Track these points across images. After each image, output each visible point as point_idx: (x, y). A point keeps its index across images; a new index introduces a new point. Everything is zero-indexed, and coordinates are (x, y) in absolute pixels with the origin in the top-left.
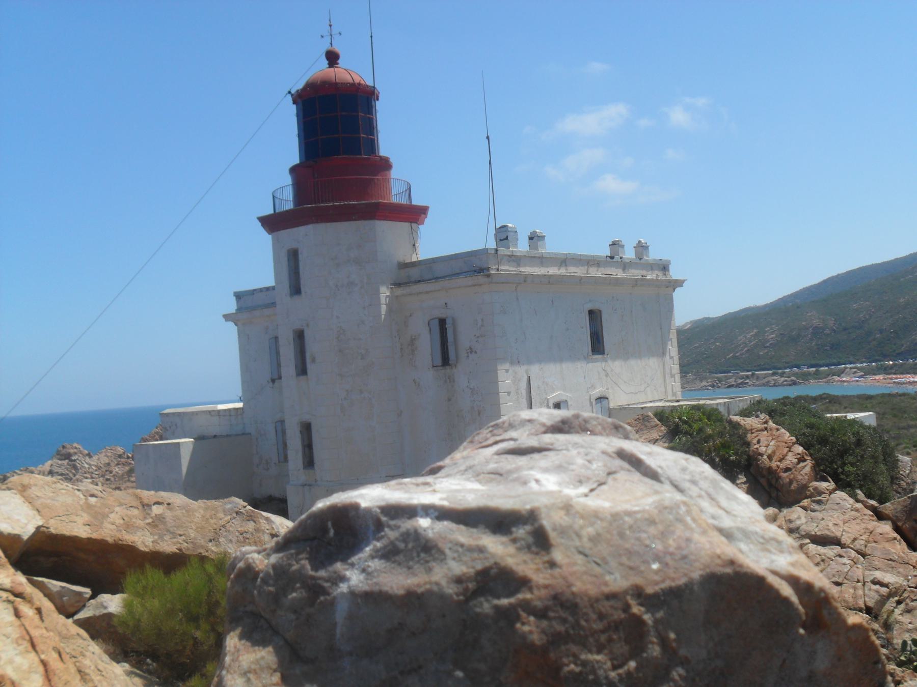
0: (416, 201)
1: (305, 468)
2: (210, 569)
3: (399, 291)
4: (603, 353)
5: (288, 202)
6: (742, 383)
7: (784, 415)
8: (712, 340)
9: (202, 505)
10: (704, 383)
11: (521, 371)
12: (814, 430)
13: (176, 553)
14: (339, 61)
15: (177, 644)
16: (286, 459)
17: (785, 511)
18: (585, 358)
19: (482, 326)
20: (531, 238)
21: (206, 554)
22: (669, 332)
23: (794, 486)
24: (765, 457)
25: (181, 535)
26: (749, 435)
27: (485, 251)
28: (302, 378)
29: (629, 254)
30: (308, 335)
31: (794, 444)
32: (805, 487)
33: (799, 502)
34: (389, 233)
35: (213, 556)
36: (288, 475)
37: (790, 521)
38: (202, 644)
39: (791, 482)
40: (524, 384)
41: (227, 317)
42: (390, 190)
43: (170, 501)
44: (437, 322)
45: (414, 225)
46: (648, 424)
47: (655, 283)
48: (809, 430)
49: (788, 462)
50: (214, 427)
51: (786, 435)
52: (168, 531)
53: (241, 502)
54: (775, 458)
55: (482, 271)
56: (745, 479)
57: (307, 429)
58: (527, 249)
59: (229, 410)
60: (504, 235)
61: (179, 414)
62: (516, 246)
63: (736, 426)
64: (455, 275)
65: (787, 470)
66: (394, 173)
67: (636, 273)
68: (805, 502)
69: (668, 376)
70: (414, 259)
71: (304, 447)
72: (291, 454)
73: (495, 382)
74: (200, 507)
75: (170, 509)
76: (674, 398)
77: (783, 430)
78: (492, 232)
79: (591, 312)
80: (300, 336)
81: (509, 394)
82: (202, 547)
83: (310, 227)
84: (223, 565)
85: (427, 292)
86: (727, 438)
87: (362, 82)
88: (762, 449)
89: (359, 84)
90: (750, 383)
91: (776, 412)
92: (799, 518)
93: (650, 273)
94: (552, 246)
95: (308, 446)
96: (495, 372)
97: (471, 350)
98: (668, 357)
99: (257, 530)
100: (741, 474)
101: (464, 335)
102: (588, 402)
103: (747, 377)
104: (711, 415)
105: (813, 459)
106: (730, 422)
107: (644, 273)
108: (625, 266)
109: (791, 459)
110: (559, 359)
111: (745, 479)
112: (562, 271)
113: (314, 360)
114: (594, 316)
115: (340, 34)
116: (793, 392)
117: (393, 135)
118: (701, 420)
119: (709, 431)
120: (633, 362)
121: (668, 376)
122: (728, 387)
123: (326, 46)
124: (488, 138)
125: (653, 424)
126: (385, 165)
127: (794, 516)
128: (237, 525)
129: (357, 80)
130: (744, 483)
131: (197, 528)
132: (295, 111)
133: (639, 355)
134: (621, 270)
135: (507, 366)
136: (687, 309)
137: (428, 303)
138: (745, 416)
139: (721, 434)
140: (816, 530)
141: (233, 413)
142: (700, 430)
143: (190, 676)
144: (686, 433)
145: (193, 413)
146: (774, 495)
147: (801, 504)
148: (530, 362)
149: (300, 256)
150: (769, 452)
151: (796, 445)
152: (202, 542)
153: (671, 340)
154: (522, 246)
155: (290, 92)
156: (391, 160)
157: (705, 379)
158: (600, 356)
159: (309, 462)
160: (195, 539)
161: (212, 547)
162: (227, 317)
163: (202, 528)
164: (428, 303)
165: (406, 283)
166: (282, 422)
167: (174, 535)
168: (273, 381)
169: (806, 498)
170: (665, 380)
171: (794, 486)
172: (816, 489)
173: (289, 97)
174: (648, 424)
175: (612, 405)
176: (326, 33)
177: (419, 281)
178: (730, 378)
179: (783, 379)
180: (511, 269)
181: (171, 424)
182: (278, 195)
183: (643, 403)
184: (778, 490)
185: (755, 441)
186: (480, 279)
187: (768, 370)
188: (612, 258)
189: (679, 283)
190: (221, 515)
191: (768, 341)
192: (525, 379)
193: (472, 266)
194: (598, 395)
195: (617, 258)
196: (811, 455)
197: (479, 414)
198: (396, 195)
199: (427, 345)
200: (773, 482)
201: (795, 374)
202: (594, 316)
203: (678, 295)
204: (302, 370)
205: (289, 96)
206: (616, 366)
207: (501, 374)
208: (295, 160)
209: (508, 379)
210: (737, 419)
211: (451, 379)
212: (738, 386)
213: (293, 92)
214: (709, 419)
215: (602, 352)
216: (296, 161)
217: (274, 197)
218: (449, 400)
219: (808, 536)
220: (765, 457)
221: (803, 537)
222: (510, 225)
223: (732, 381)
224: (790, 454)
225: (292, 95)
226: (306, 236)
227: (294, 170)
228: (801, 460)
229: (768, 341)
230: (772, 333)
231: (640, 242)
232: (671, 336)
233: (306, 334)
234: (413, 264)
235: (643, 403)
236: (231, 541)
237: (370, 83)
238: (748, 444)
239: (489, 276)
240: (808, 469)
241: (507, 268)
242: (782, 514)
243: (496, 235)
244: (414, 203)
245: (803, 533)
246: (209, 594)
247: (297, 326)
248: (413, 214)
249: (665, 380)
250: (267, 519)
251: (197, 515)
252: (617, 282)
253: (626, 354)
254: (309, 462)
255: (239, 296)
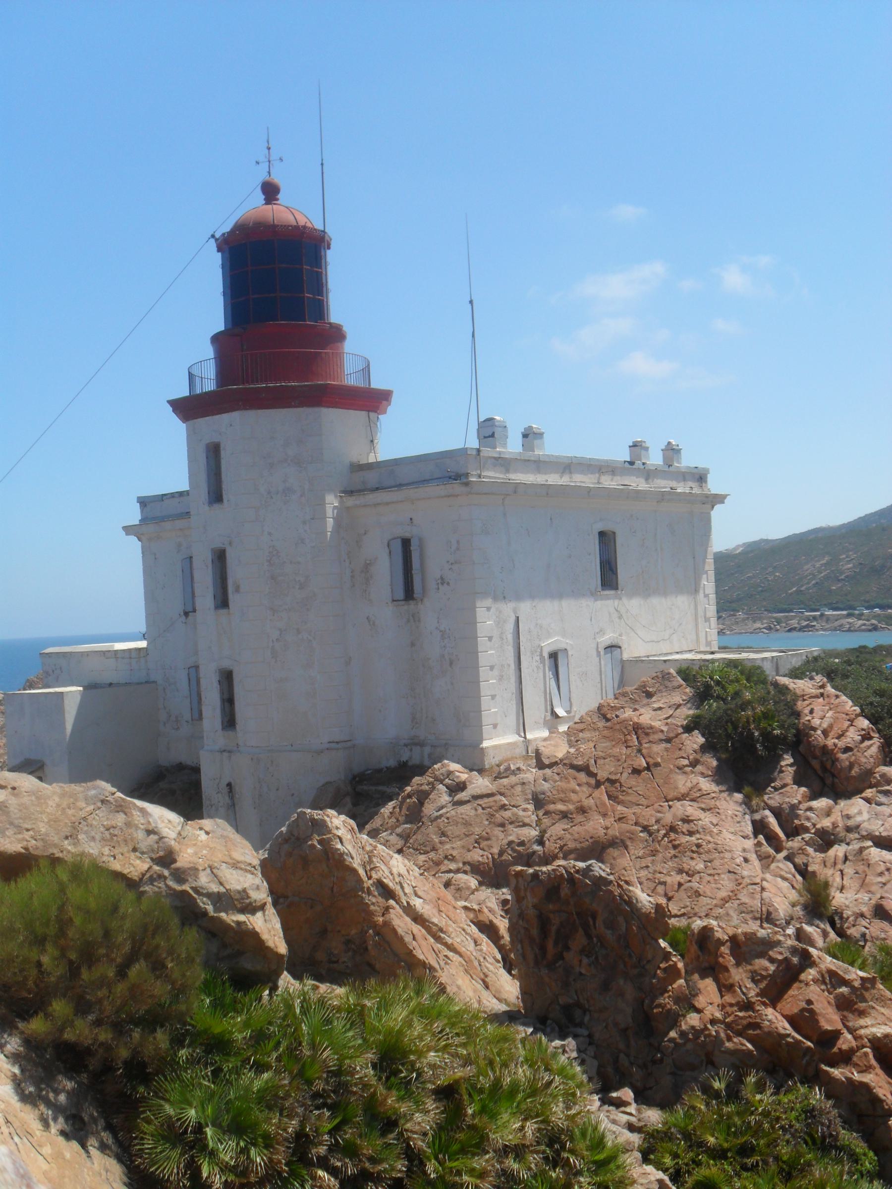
0: (377, 383)
1: (223, 729)
2: (64, 876)
3: (350, 501)
4: (617, 589)
5: (208, 383)
6: (807, 626)
7: (847, 677)
8: (770, 569)
9: (58, 790)
10: (758, 625)
11: (507, 609)
12: (884, 699)
13: (20, 854)
14: (279, 196)
15: (15, 973)
16: (200, 717)
17: (842, 803)
18: (592, 594)
19: (458, 549)
20: (525, 436)
21: (61, 855)
22: (704, 562)
23: (855, 772)
24: (819, 732)
25: (28, 830)
26: (799, 703)
27: (464, 451)
28: (223, 611)
29: (655, 458)
30: (230, 555)
31: (857, 716)
32: (870, 773)
33: (861, 792)
34: (337, 422)
35: (68, 858)
36: (202, 737)
37: (848, 817)
38: (49, 974)
39: (851, 766)
40: (510, 627)
41: (128, 530)
42: (341, 366)
43: (16, 785)
44: (399, 542)
45: (372, 415)
46: (669, 684)
47: (688, 498)
48: (878, 699)
49: (849, 740)
50: (110, 673)
51: (848, 705)
52: (11, 824)
53: (108, 787)
54: (831, 734)
55: (459, 477)
56: (792, 760)
57: (227, 678)
58: (519, 449)
59: (130, 650)
60: (489, 431)
61: (64, 654)
62: (505, 445)
63: (783, 690)
64: (424, 482)
65: (847, 749)
66: (349, 346)
67: (663, 484)
68: (869, 793)
69: (701, 620)
70: (371, 459)
71: (223, 701)
72: (207, 711)
73: (472, 623)
74: (54, 793)
75: (15, 795)
76: (708, 649)
77: (844, 698)
78: (474, 427)
79: (602, 534)
80: (220, 557)
81: (490, 639)
82: (56, 846)
83: (236, 415)
84: (83, 872)
85: (387, 504)
86: (771, 705)
87: (309, 225)
88: (816, 722)
89: (305, 227)
90: (818, 626)
91: (835, 671)
92: (860, 813)
93: (681, 484)
94: (552, 447)
95: (228, 701)
96: (473, 609)
97: (443, 581)
98: (701, 595)
99: (128, 824)
100: (787, 753)
101: (434, 562)
102: (595, 653)
103: (815, 618)
104: (752, 674)
105: (881, 737)
106: (776, 684)
107: (674, 484)
108: (649, 474)
109: (853, 736)
110: (560, 595)
111: (792, 760)
112: (565, 480)
113: (237, 589)
114: (606, 539)
115: (281, 159)
116: (871, 640)
117: (350, 295)
118: (737, 681)
119: (748, 695)
120: (655, 601)
121: (701, 620)
122: (790, 630)
123: (262, 176)
124: (471, 302)
125: (675, 684)
126: (336, 335)
127: (853, 811)
128: (102, 818)
129: (302, 221)
130: (791, 765)
131: (49, 821)
132: (220, 262)
133: (664, 592)
134: (642, 480)
135: (488, 602)
136: (729, 531)
137: (387, 517)
138: (797, 677)
139: (763, 701)
140: (882, 829)
141: (134, 655)
142: (737, 694)
143: (32, 1016)
144: (719, 698)
145: (82, 654)
146: (829, 781)
147: (864, 795)
148: (518, 597)
149: (223, 453)
150: (825, 725)
151: (861, 718)
152: (56, 839)
153: (706, 573)
154: (513, 446)
155: (213, 236)
156: (344, 329)
157: (760, 619)
158: (612, 592)
159: (230, 722)
160: (47, 835)
161: (67, 845)
162: (128, 530)
163: (56, 820)
164: (387, 517)
165: (360, 491)
166: (197, 667)
167: (19, 829)
168: (186, 614)
169: (871, 787)
170: (697, 625)
171: (855, 772)
172: (883, 776)
173: (213, 244)
174: (669, 684)
175: (626, 656)
176: (262, 159)
177: (377, 489)
178: (793, 618)
179: (861, 622)
180: (497, 475)
181: (55, 667)
182: (195, 372)
183: (667, 654)
184: (833, 776)
185: (807, 711)
186: (456, 487)
187: (842, 610)
188: (631, 463)
189: (719, 499)
190: (82, 804)
191: (842, 573)
192: (512, 620)
193: (446, 472)
194: (608, 643)
195: (638, 463)
196: (879, 731)
197: (451, 664)
198: (350, 375)
199: (385, 572)
200: (829, 766)
201: (876, 617)
202: (606, 539)
203: (718, 514)
204: (223, 602)
205: (213, 240)
206: (633, 605)
207: (481, 613)
208: (218, 324)
209: (490, 620)
210: (784, 680)
211: (415, 618)
212: (802, 629)
213: (218, 235)
214: (748, 680)
215: (616, 588)
216: (221, 327)
217: (191, 376)
218: (413, 644)
219: (871, 837)
220: (819, 732)
221: (863, 838)
222: (497, 418)
223: (794, 623)
224: (852, 729)
225: (216, 240)
226: (231, 426)
227: (216, 339)
228: (866, 737)
229: (842, 573)
230: (849, 562)
231: (669, 443)
232: (707, 568)
233: (228, 554)
234: (369, 467)
235: (667, 654)
236: (93, 839)
237: (319, 226)
238: (798, 715)
239: (467, 484)
240: (874, 750)
241: (492, 475)
242: (838, 806)
243: (478, 430)
244: (373, 386)
245: (865, 833)
246: (61, 908)
247: (218, 544)
248: (372, 401)
249: (697, 625)
250: (143, 811)
251: (50, 803)
252: (638, 495)
253: (646, 590)
254: (230, 722)
255: (144, 502)
